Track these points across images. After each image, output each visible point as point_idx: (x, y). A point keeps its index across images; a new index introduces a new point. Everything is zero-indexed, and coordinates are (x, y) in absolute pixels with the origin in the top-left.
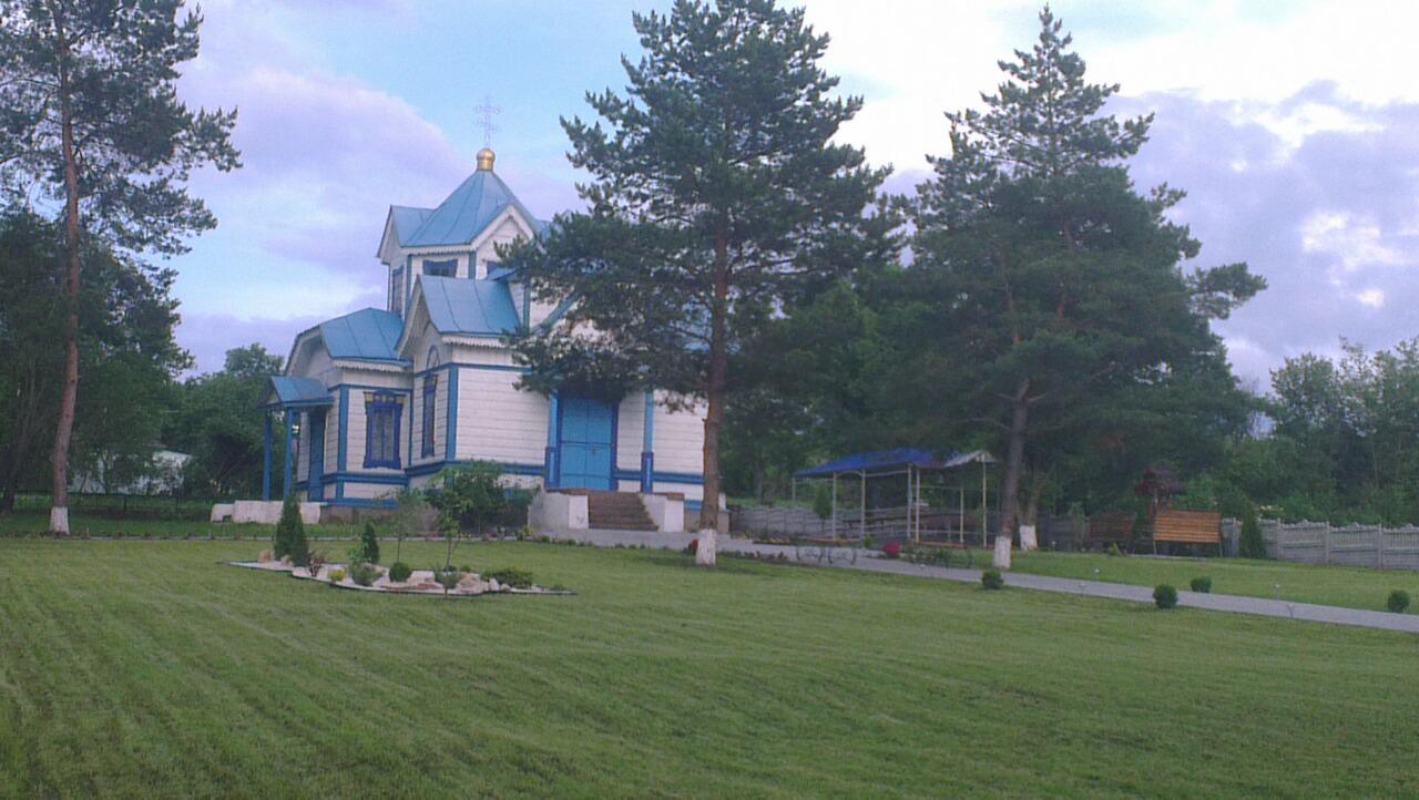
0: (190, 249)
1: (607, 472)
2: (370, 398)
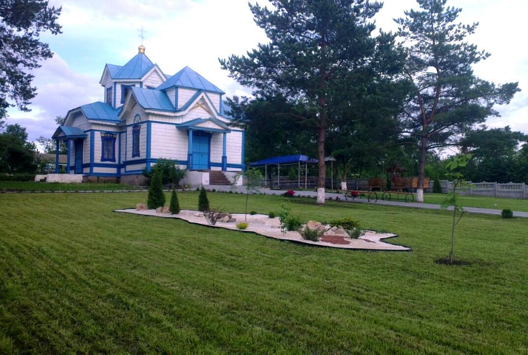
0: (41, 66)
1: (206, 163)
2: (103, 135)
